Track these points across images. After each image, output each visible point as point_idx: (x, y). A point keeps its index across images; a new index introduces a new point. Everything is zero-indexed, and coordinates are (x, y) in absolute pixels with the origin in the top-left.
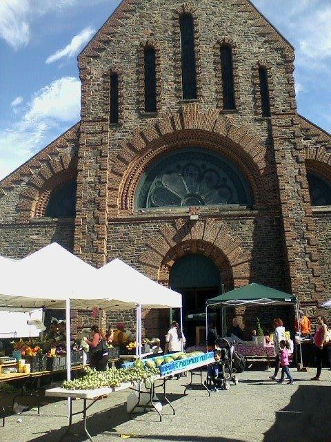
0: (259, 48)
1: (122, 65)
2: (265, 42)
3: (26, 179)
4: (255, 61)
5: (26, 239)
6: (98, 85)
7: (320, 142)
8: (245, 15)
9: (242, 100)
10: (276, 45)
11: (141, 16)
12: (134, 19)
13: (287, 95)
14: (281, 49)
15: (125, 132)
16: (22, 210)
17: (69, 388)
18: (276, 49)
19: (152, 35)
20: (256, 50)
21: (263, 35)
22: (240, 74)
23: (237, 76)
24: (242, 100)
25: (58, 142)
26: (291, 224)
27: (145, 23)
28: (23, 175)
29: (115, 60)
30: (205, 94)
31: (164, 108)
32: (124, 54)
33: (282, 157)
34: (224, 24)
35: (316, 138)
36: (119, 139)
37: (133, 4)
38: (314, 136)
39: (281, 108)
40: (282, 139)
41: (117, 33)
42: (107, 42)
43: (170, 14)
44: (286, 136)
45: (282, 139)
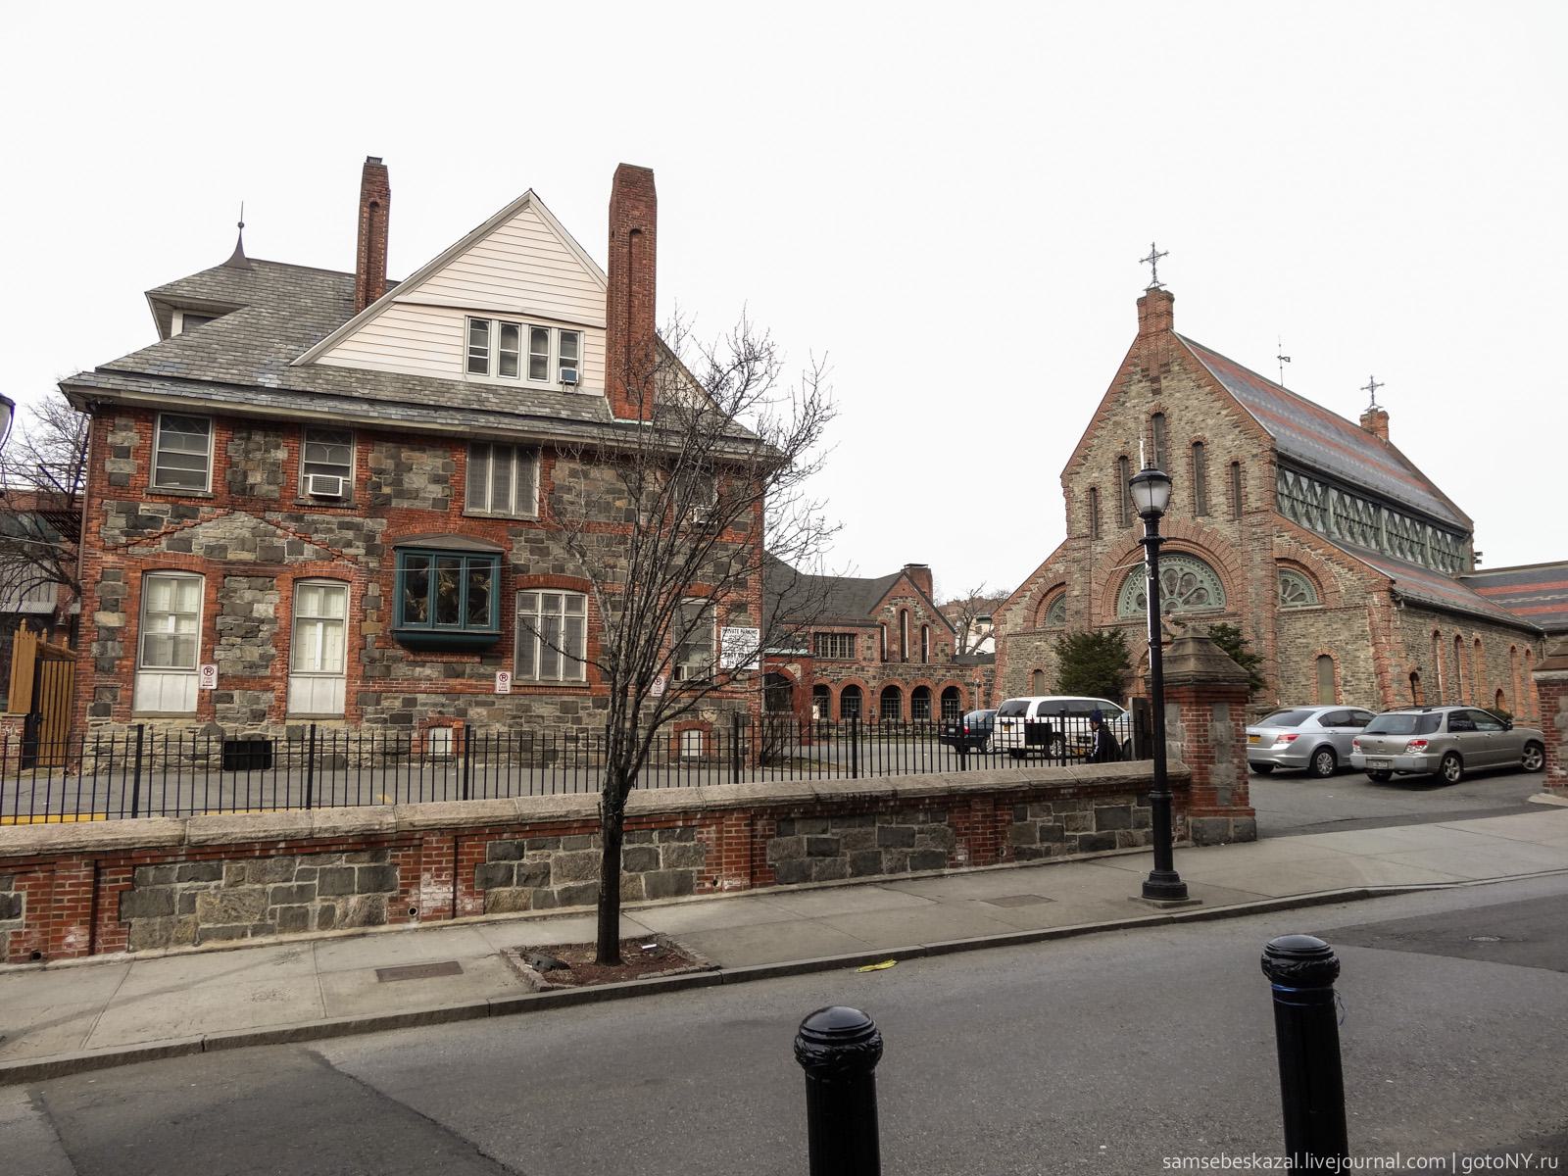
0: (1233, 441)
2: (1240, 432)
4: (1227, 458)
8: (1219, 404)
9: (1213, 502)
24: (1213, 502)
39: (1254, 505)
43: (1143, 417)
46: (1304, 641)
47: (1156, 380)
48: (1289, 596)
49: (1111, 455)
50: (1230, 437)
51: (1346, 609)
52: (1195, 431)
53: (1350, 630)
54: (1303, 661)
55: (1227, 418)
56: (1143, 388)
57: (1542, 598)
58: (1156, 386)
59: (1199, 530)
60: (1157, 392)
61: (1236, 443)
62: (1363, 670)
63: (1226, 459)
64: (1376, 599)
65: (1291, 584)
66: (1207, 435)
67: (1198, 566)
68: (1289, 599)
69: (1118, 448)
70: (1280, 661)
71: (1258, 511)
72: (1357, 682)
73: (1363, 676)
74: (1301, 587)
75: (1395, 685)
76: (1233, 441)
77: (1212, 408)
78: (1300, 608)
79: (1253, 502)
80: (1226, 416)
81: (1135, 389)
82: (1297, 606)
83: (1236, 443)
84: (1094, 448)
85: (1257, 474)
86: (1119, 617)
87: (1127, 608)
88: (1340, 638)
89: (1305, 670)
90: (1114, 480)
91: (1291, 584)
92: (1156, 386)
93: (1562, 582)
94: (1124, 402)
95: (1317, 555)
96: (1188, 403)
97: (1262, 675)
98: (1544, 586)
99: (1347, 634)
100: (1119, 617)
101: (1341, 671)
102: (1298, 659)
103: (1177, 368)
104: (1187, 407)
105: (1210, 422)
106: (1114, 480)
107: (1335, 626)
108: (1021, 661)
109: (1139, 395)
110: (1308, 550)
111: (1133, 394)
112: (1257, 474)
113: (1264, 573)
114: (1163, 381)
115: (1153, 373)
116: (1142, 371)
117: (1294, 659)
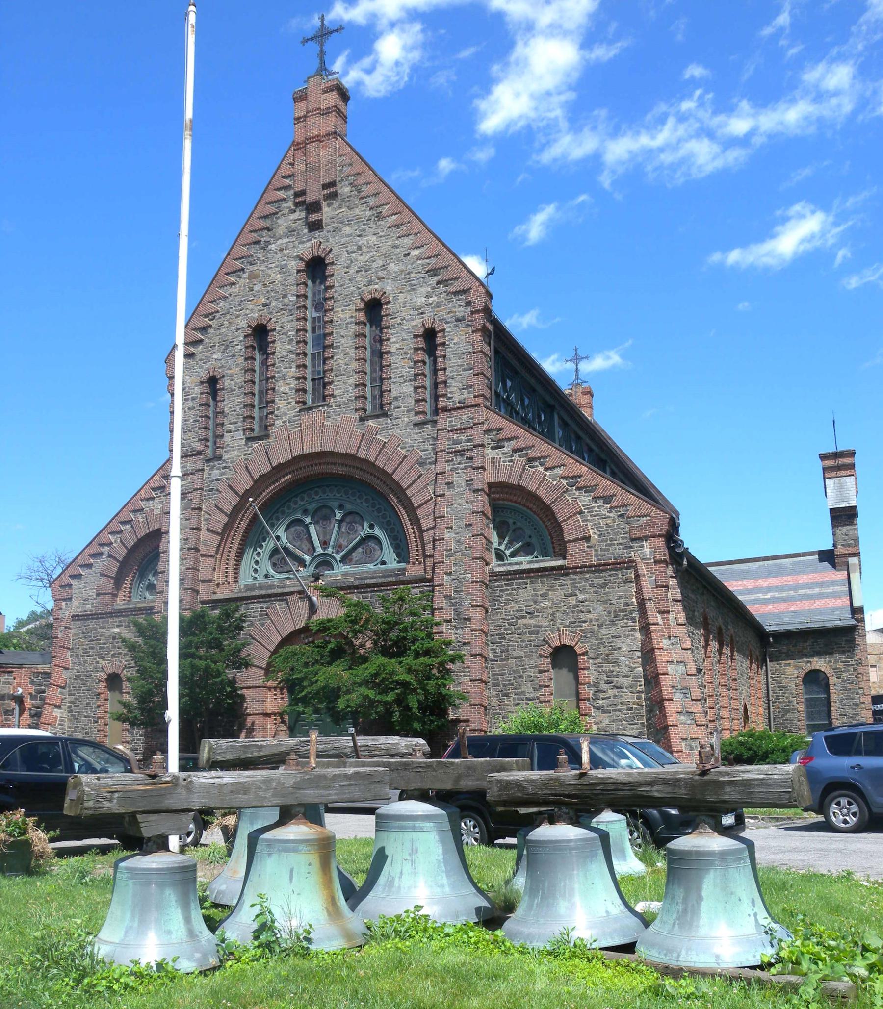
0: (428, 296)
1: (223, 362)
2: (439, 283)
3: (106, 549)
4: (418, 322)
5: (107, 634)
6: (193, 399)
7: (521, 450)
8: (407, 241)
9: (394, 393)
10: (456, 286)
11: (252, 276)
12: (243, 281)
13: (327, 380)
14: (464, 292)
15: (225, 468)
16: (102, 594)
17: (510, 564)
18: (456, 293)
19: (265, 305)
20: (420, 301)
21: (433, 272)
22: (393, 350)
23: (388, 352)
24: (394, 393)
25: (142, 492)
26: (446, 597)
27: (256, 288)
28: (102, 545)
29: (215, 356)
30: (336, 392)
31: (278, 423)
32: (226, 345)
33: (447, 484)
34: (374, 265)
35: (513, 443)
36: (217, 480)
37: (240, 259)
38: (509, 439)
39: (457, 397)
40: (451, 453)
41: (218, 312)
42: (204, 329)
43: (294, 265)
44: (459, 447)
45: (451, 453)
46: (532, 622)
47: (314, 207)
48: (507, 548)
49: (243, 323)
50: (424, 290)
51: (599, 568)
52: (370, 283)
53: (605, 602)
54: (529, 657)
55: (419, 262)
56: (295, 221)
57: (761, 596)
58: (314, 217)
59: (368, 438)
60: (315, 226)
61: (431, 300)
62: (625, 670)
63: (416, 324)
64: (647, 550)
65: (512, 527)
66: (389, 289)
67: (367, 501)
68: (508, 552)
69: (254, 314)
70: (492, 656)
71: (462, 406)
72: (615, 691)
73: (626, 682)
74: (528, 532)
75: (678, 696)
76: (428, 296)
77: (396, 247)
78: (525, 566)
79: (455, 393)
80: (419, 258)
81: (283, 224)
82: (521, 563)
83: (431, 300)
84: (218, 315)
85: (464, 347)
86: (242, 583)
87: (256, 571)
88: (590, 616)
89: (531, 673)
90: (245, 364)
91: (512, 527)
92: (314, 217)
93: (780, 579)
94: (268, 243)
95: (554, 477)
96: (362, 241)
97: (361, 316)
98: (762, 583)
99: (600, 608)
100: (242, 583)
101: (590, 675)
102: (522, 653)
103: (347, 190)
104: (360, 248)
105: (393, 267)
106: (245, 364)
107: (581, 597)
108: (88, 659)
109: (291, 232)
110: (541, 469)
111: (281, 231)
112: (464, 347)
113: (469, 506)
114: (325, 209)
115: (310, 198)
116: (297, 195)
117: (515, 654)
